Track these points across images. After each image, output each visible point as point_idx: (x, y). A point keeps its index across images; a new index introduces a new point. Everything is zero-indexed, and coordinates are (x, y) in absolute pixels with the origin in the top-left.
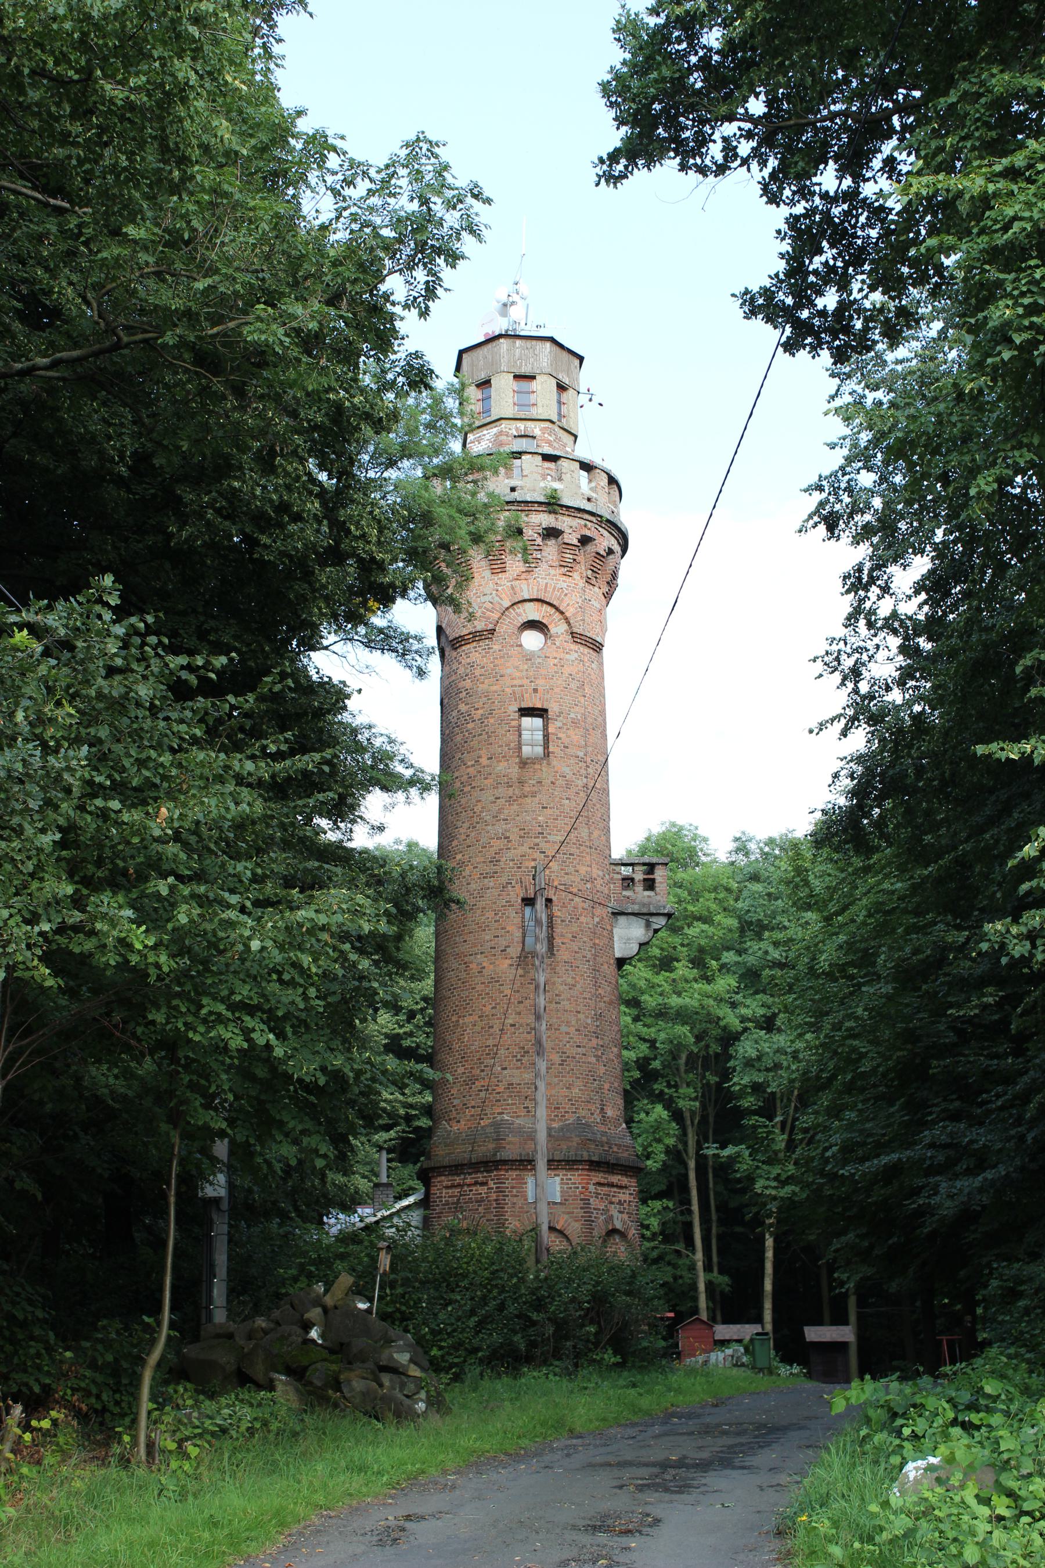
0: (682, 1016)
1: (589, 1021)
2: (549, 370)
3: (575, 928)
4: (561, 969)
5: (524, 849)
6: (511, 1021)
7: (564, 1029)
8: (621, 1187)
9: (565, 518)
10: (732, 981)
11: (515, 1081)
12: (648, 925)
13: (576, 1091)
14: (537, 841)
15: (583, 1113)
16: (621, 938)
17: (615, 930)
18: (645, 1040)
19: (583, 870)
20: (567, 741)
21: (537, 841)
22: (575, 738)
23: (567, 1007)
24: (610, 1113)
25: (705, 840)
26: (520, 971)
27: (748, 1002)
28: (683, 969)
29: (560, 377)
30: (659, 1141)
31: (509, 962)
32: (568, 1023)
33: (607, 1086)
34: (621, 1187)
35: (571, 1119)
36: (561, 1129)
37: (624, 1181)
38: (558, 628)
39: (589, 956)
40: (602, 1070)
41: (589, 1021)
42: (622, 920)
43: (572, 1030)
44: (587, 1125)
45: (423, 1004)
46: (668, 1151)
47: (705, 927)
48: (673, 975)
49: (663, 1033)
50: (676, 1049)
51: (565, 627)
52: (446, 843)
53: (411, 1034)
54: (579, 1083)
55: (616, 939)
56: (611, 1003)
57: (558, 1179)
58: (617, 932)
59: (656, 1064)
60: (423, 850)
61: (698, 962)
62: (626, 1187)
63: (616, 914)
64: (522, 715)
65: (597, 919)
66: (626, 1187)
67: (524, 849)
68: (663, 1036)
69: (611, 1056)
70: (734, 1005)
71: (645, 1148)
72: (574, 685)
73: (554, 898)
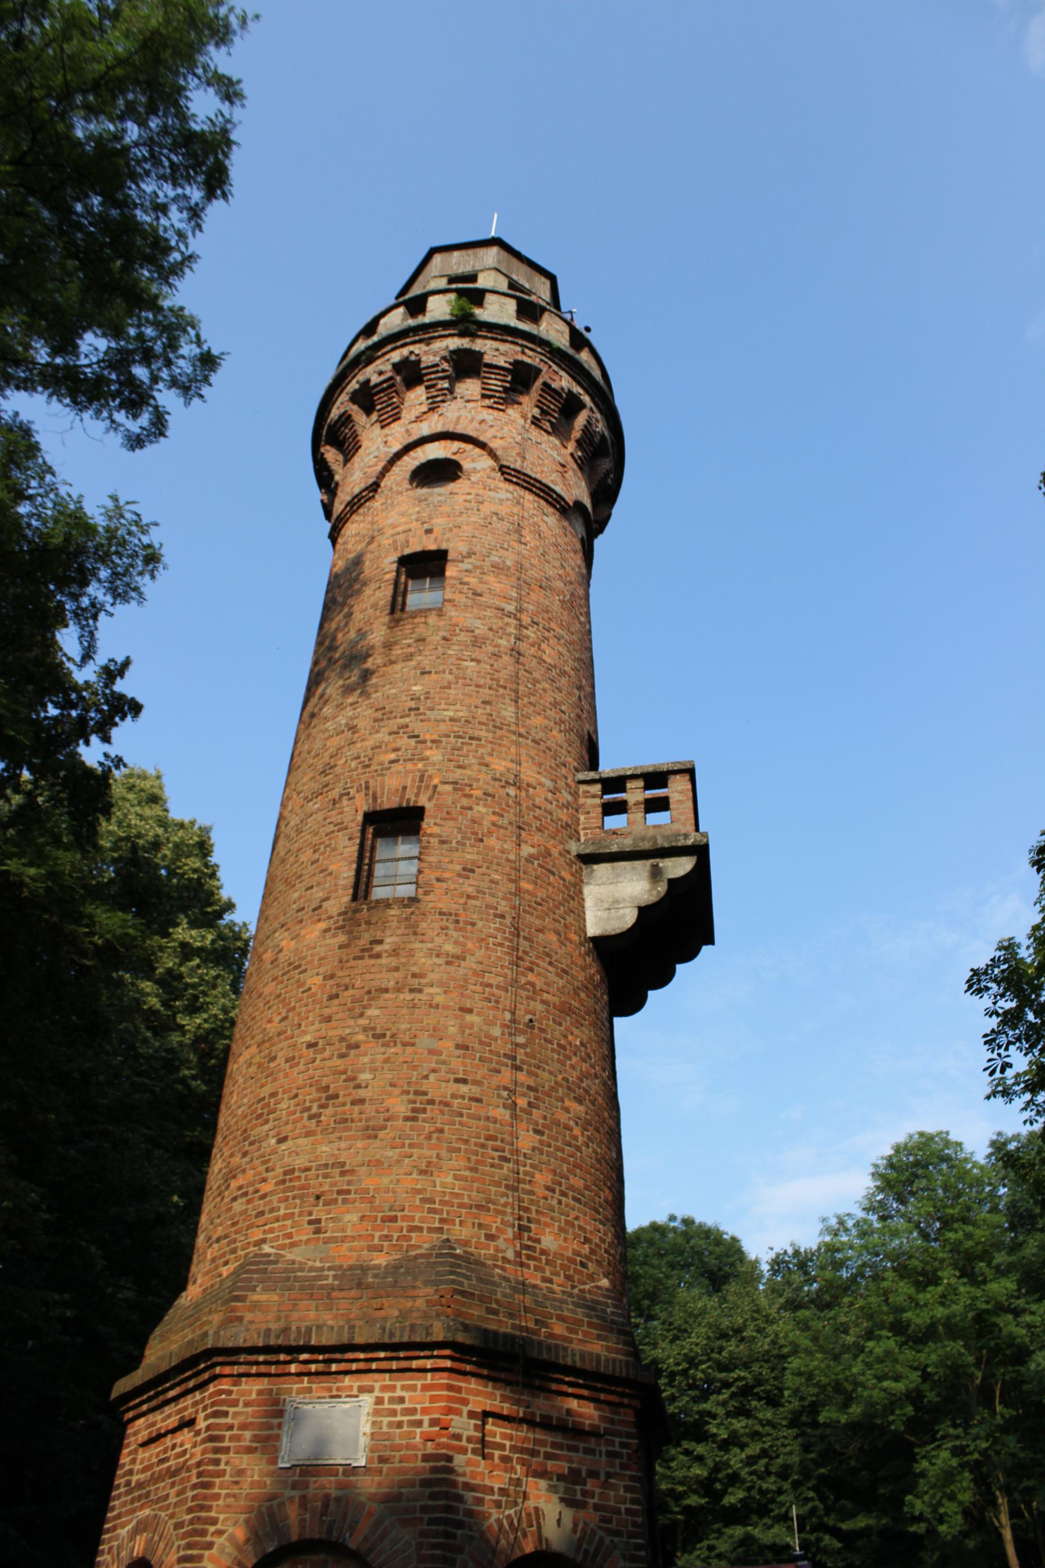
0: (952, 1329)
1: (496, 1031)
2: (496, 265)
3: (471, 855)
4: (429, 926)
5: (382, 736)
6: (308, 1038)
7: (425, 1041)
9: (489, 343)
10: (1008, 1285)
11: (300, 1162)
12: (656, 874)
13: (445, 1180)
14: (403, 721)
15: (460, 1232)
16: (599, 901)
17: (587, 890)
18: (916, 1369)
19: (500, 765)
20: (480, 588)
21: (403, 721)
22: (497, 587)
23: (440, 999)
24: (549, 1241)
25: (959, 1144)
26: (342, 938)
27: (1033, 1307)
28: (948, 1276)
29: (514, 277)
30: (952, 1497)
31: (323, 925)
32: (437, 1033)
33: (542, 1178)
35: (423, 1242)
36: (393, 1269)
38: (475, 462)
39: (503, 907)
40: (526, 1140)
41: (496, 1031)
42: (602, 870)
43: (447, 1046)
44: (467, 1258)
45: (685, 1365)
46: (966, 1513)
47: (969, 1228)
48: (940, 1289)
49: (931, 1355)
50: (956, 1371)
51: (487, 462)
52: (615, 1113)
54: (457, 1162)
55: (589, 903)
56: (566, 1010)
57: (367, 1401)
58: (591, 893)
59: (931, 1396)
60: (700, 1226)
61: (968, 1273)
62: (594, 1433)
63: (590, 859)
64: (412, 575)
65: (527, 850)
67: (382, 736)
68: (934, 1357)
69: (563, 1117)
70: (1017, 1313)
71: (935, 1510)
72: (500, 526)
73: (428, 805)
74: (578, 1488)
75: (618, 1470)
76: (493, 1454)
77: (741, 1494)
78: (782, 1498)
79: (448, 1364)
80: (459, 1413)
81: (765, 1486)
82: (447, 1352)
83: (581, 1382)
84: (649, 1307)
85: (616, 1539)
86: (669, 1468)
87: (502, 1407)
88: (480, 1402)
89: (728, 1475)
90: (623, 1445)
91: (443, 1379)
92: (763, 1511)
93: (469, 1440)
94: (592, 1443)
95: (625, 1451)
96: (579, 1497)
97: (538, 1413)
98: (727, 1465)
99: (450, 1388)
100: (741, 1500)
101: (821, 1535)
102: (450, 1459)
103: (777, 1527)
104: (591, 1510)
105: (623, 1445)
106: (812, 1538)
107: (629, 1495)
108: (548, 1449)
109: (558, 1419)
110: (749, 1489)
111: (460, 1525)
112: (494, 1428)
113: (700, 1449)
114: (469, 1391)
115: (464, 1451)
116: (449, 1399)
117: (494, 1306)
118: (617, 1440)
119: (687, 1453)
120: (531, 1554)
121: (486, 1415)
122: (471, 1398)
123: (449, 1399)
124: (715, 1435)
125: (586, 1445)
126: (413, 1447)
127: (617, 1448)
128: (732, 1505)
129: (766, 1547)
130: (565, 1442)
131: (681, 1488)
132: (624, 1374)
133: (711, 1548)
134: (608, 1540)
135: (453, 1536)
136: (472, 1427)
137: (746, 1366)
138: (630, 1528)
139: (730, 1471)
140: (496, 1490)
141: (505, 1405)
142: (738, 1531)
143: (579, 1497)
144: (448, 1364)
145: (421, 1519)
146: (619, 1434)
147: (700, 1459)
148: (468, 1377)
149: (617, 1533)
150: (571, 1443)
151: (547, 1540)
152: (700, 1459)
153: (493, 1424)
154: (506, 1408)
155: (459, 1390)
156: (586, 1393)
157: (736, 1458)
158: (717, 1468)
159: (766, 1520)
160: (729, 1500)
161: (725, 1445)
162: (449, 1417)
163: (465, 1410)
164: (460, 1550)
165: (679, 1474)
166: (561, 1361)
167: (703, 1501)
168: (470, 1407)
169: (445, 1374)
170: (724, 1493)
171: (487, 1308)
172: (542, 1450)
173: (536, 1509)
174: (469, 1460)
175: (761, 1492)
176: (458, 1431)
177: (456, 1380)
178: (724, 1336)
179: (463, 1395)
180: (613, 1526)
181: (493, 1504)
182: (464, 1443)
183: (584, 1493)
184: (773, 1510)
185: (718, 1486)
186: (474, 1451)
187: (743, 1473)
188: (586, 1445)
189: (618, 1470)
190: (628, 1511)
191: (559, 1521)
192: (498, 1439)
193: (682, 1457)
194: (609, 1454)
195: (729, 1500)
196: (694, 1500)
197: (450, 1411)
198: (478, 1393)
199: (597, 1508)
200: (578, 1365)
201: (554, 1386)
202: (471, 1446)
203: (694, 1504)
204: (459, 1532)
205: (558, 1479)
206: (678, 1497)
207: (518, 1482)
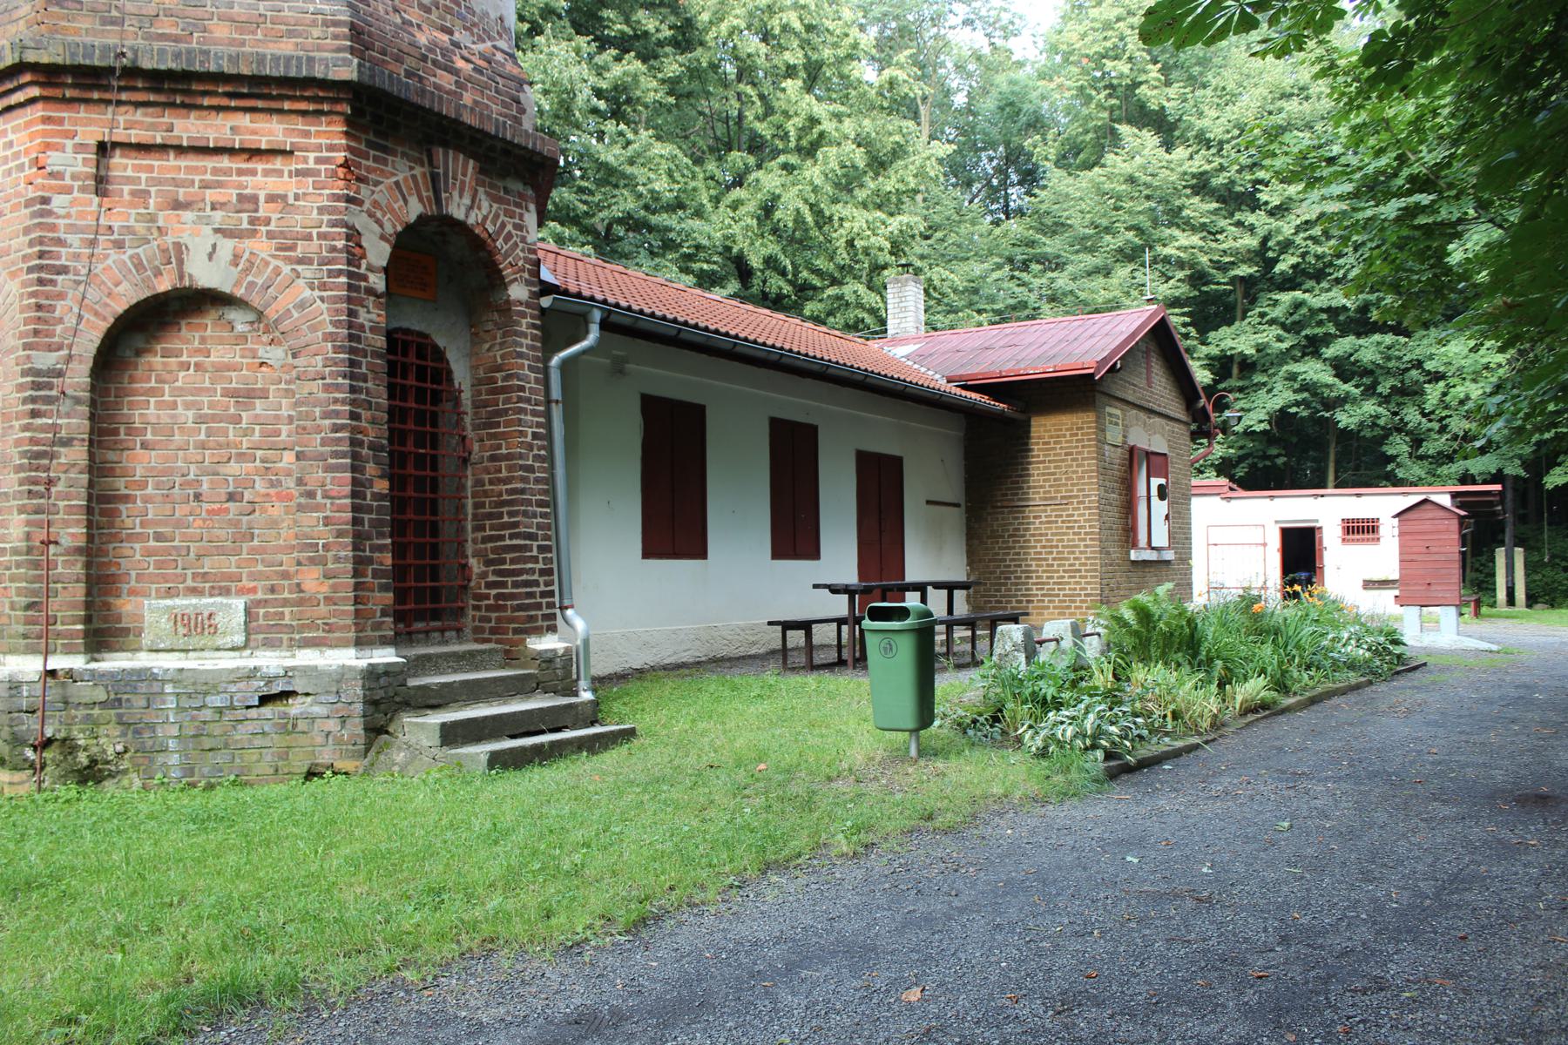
8: (254, 153)
34: (254, 153)
37: (270, 130)
53: (1222, 168)
62: (286, 153)
66: (286, 153)
74: (245, 216)
75: (311, 190)
76: (122, 190)
77: (1294, 260)
78: (1341, 261)
79: (35, 92)
80: (62, 149)
81: (1320, 250)
82: (27, 78)
83: (245, 91)
84: (1201, 74)
85: (299, 268)
86: (1217, 240)
87: (130, 135)
88: (92, 132)
89: (1278, 243)
90: (318, 161)
91: (38, 111)
92: (1319, 276)
93: (74, 177)
94: (278, 163)
95: (323, 167)
96: (245, 225)
97: (185, 136)
98: (1278, 231)
99: (46, 120)
100: (1294, 267)
101: (1382, 295)
102: (45, 201)
103: (1334, 290)
104: (264, 239)
105: (318, 161)
106: (1373, 297)
107: (326, 218)
108: (208, 177)
109: (216, 139)
110: (1303, 255)
111: (63, 270)
112: (125, 161)
113: (1251, 218)
114: (75, 122)
115: (68, 190)
116: (45, 133)
117: (114, 13)
118: (312, 156)
119: (1239, 224)
120: (166, 293)
121: (103, 149)
122: (79, 129)
123: (45, 133)
124: (1266, 203)
125: (269, 166)
126: (18, 194)
127: (311, 165)
128: (1282, 273)
129: (1322, 310)
130: (234, 166)
131: (1227, 259)
132: (304, 73)
133: (1262, 315)
134: (286, 269)
135: (53, 282)
136: (80, 161)
137: (1309, 126)
138: (325, 254)
139: (1280, 238)
140: (116, 229)
141: (133, 132)
142: (1286, 298)
143: (245, 225)
144: (35, 92)
145: (21, 269)
146: (319, 148)
147: (1251, 229)
148: (77, 105)
149: (300, 261)
150: (244, 166)
151: (190, 276)
152: (1251, 229)
153: (122, 156)
154: (135, 136)
155: (61, 121)
156: (260, 104)
157: (1286, 228)
158: (1265, 240)
159: (1324, 285)
160: (1281, 267)
161: (1279, 211)
162: (49, 153)
163: (69, 143)
164: (61, 296)
165: (1225, 246)
166: (197, 68)
167: (1251, 270)
168: (77, 140)
169: (40, 106)
170: (1275, 261)
171: (101, 17)
172: (197, 178)
173: (178, 246)
174: (75, 199)
175: (1318, 257)
176: (56, 169)
177: (57, 111)
178: (1286, 96)
179: (67, 127)
180: (299, 253)
181: (111, 245)
182: (68, 181)
183: (252, 221)
184: (1330, 274)
185: (1270, 254)
186: (83, 189)
187: (1298, 240)
188: (269, 166)
189: (311, 190)
190: (321, 236)
191: (210, 256)
192: (129, 173)
193: (1233, 229)
194: (299, 173)
195: (1281, 267)
196: (1244, 270)
197: (48, 147)
198: (89, 122)
199: (270, 235)
200: (226, 70)
201: (206, 102)
202: (77, 184)
203: (1242, 274)
204: (60, 278)
205: (213, 208)
206: (1222, 267)
207: (152, 218)
